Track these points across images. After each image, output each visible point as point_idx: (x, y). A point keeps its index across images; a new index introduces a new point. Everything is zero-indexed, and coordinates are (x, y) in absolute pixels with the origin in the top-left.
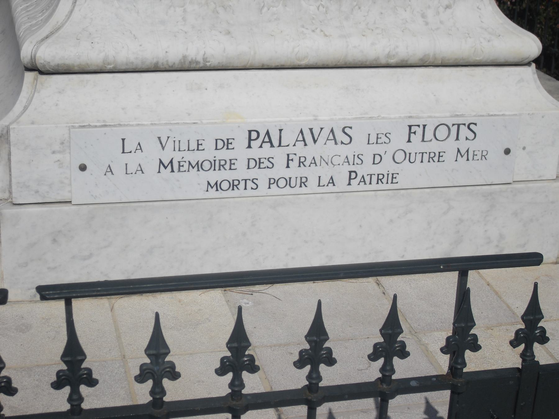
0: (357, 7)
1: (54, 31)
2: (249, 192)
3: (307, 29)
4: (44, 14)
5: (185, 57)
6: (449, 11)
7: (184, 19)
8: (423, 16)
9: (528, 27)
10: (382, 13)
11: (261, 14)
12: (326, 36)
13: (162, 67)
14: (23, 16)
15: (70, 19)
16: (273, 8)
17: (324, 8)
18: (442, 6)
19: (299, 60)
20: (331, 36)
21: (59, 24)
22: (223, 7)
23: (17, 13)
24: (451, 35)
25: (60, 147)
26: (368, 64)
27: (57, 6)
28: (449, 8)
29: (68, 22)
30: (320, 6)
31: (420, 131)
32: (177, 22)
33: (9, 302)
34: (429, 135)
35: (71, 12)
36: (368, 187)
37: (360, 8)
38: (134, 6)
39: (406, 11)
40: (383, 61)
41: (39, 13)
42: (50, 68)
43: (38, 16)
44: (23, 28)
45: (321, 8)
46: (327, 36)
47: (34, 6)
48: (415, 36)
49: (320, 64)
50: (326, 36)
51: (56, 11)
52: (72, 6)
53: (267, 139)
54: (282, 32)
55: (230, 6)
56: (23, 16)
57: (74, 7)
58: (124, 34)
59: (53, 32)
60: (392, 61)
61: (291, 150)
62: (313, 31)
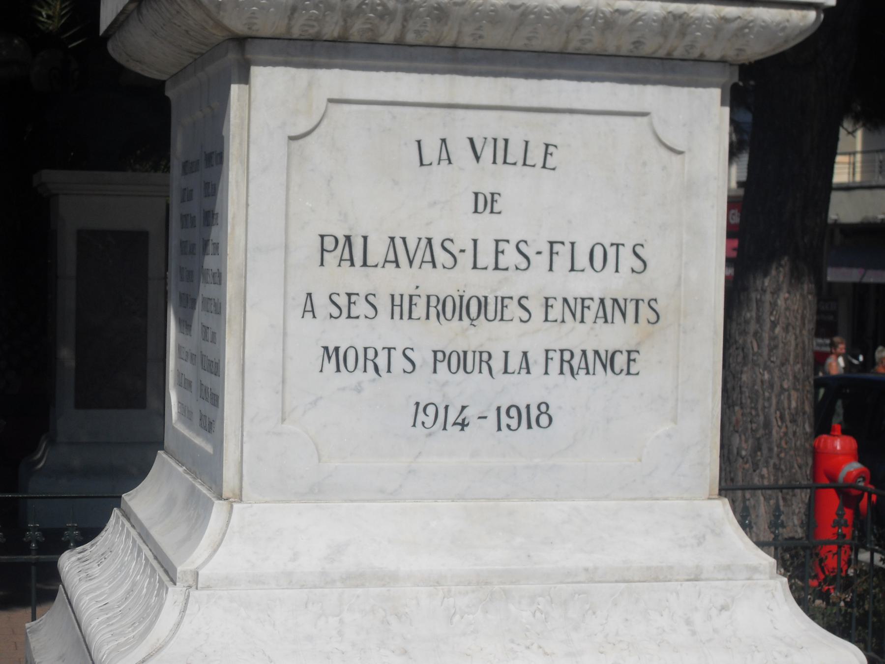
0: (590, 612)
1: (154, 652)
3: (518, 644)
4: (136, 628)
6: (725, 614)
7: (340, 633)
8: (688, 622)
9: (846, 635)
10: (627, 620)
11: (451, 625)
12: (546, 654)
14: (103, 632)
15: (177, 635)
16: (468, 615)
17: (542, 614)
18: (715, 607)
19: (313, 604)
20: (554, 654)
21: (160, 642)
22: (396, 615)
23: (93, 627)
24: (730, 648)
27: (157, 616)
28: (726, 610)
29: (174, 639)
30: (537, 611)
32: (330, 638)
35: (178, 624)
37: (594, 613)
38: (269, 616)
39: (662, 616)
41: (129, 628)
43: (127, 632)
44: (106, 649)
45: (538, 614)
46: (548, 655)
47: (120, 617)
48: (677, 652)
50: (546, 654)
51: (156, 624)
52: (179, 616)
54: (482, 650)
55: (407, 613)
56: (103, 632)
57: (182, 618)
58: (254, 656)
59: (152, 654)
62: (528, 648)
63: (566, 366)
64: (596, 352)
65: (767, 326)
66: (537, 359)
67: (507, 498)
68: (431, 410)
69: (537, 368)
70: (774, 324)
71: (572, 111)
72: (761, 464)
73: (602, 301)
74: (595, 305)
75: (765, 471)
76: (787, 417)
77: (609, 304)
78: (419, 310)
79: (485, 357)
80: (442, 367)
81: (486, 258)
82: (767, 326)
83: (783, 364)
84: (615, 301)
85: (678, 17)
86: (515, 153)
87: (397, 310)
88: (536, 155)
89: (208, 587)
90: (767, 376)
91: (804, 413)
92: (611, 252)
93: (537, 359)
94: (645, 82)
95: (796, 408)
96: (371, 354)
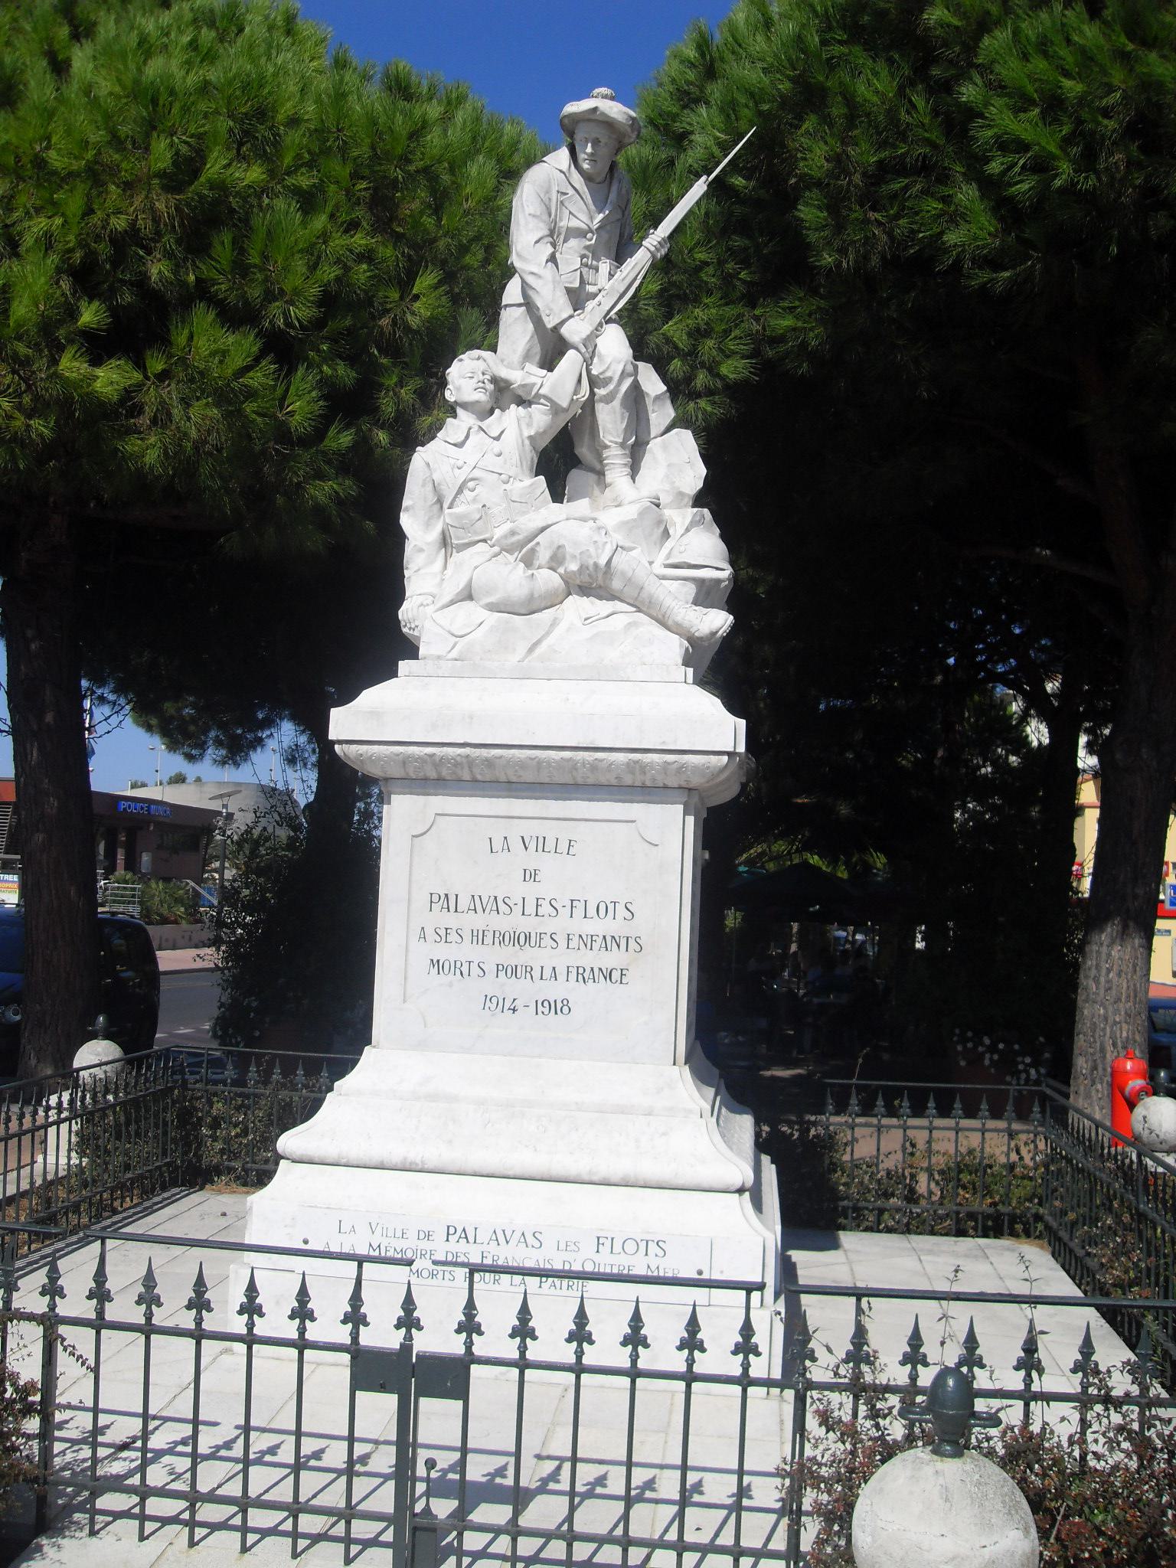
2: (446, 1283)
5: (405, 1159)
13: (387, 1166)
25: (74, 215)
26: (572, 1179)
31: (608, 1243)
33: (506, 306)
34: (617, 1248)
36: (558, 1292)
40: (586, 1178)
42: (538, 543)
49: (527, 1176)
53: (463, 1235)
60: (595, 1178)
61: (485, 1248)
63: (580, 977)
64: (600, 969)
65: (1104, 972)
66: (561, 972)
67: (540, 1056)
68: (494, 1000)
69: (562, 977)
70: (1109, 971)
71: (586, 820)
72: (1097, 1080)
73: (604, 937)
74: (600, 940)
75: (1099, 1086)
76: (1120, 1044)
77: (609, 939)
78: (489, 939)
79: (529, 969)
80: (502, 974)
81: (530, 908)
82: (1104, 972)
83: (1115, 1002)
84: (613, 937)
85: (636, 762)
86: (550, 845)
87: (475, 938)
88: (563, 847)
89: (345, 1095)
90: (1102, 1011)
91: (1135, 1041)
92: (611, 907)
93: (561, 972)
94: (632, 801)
95: (1128, 1038)
96: (458, 965)
